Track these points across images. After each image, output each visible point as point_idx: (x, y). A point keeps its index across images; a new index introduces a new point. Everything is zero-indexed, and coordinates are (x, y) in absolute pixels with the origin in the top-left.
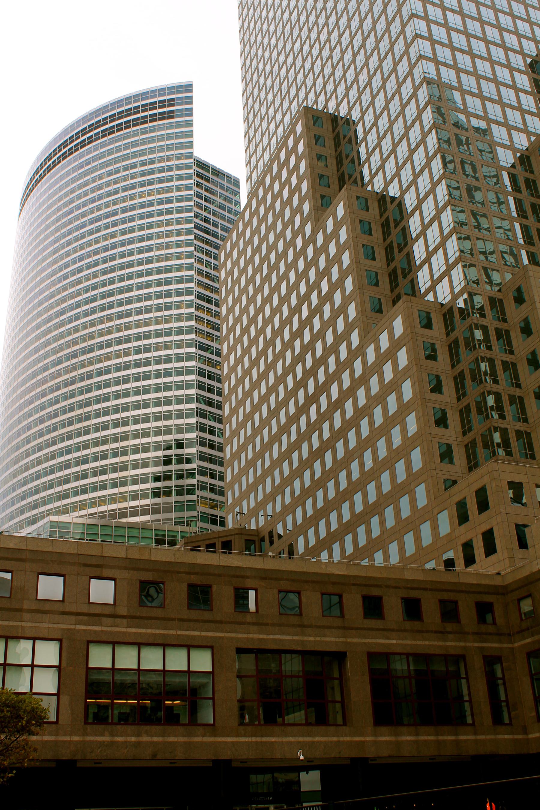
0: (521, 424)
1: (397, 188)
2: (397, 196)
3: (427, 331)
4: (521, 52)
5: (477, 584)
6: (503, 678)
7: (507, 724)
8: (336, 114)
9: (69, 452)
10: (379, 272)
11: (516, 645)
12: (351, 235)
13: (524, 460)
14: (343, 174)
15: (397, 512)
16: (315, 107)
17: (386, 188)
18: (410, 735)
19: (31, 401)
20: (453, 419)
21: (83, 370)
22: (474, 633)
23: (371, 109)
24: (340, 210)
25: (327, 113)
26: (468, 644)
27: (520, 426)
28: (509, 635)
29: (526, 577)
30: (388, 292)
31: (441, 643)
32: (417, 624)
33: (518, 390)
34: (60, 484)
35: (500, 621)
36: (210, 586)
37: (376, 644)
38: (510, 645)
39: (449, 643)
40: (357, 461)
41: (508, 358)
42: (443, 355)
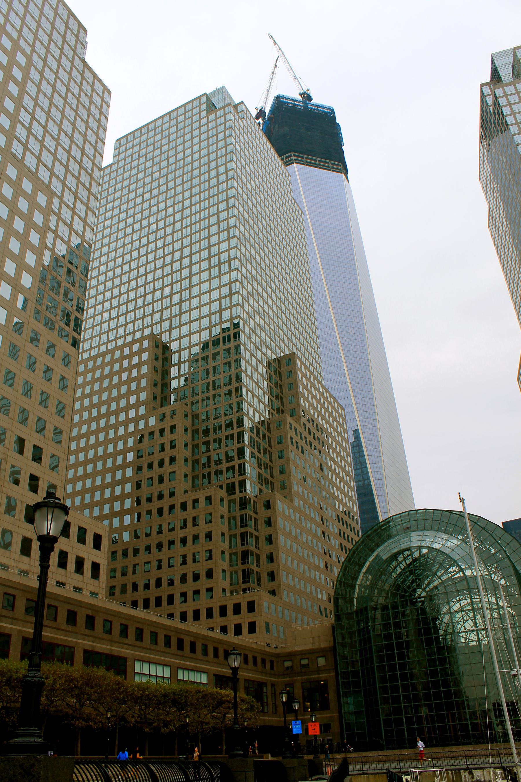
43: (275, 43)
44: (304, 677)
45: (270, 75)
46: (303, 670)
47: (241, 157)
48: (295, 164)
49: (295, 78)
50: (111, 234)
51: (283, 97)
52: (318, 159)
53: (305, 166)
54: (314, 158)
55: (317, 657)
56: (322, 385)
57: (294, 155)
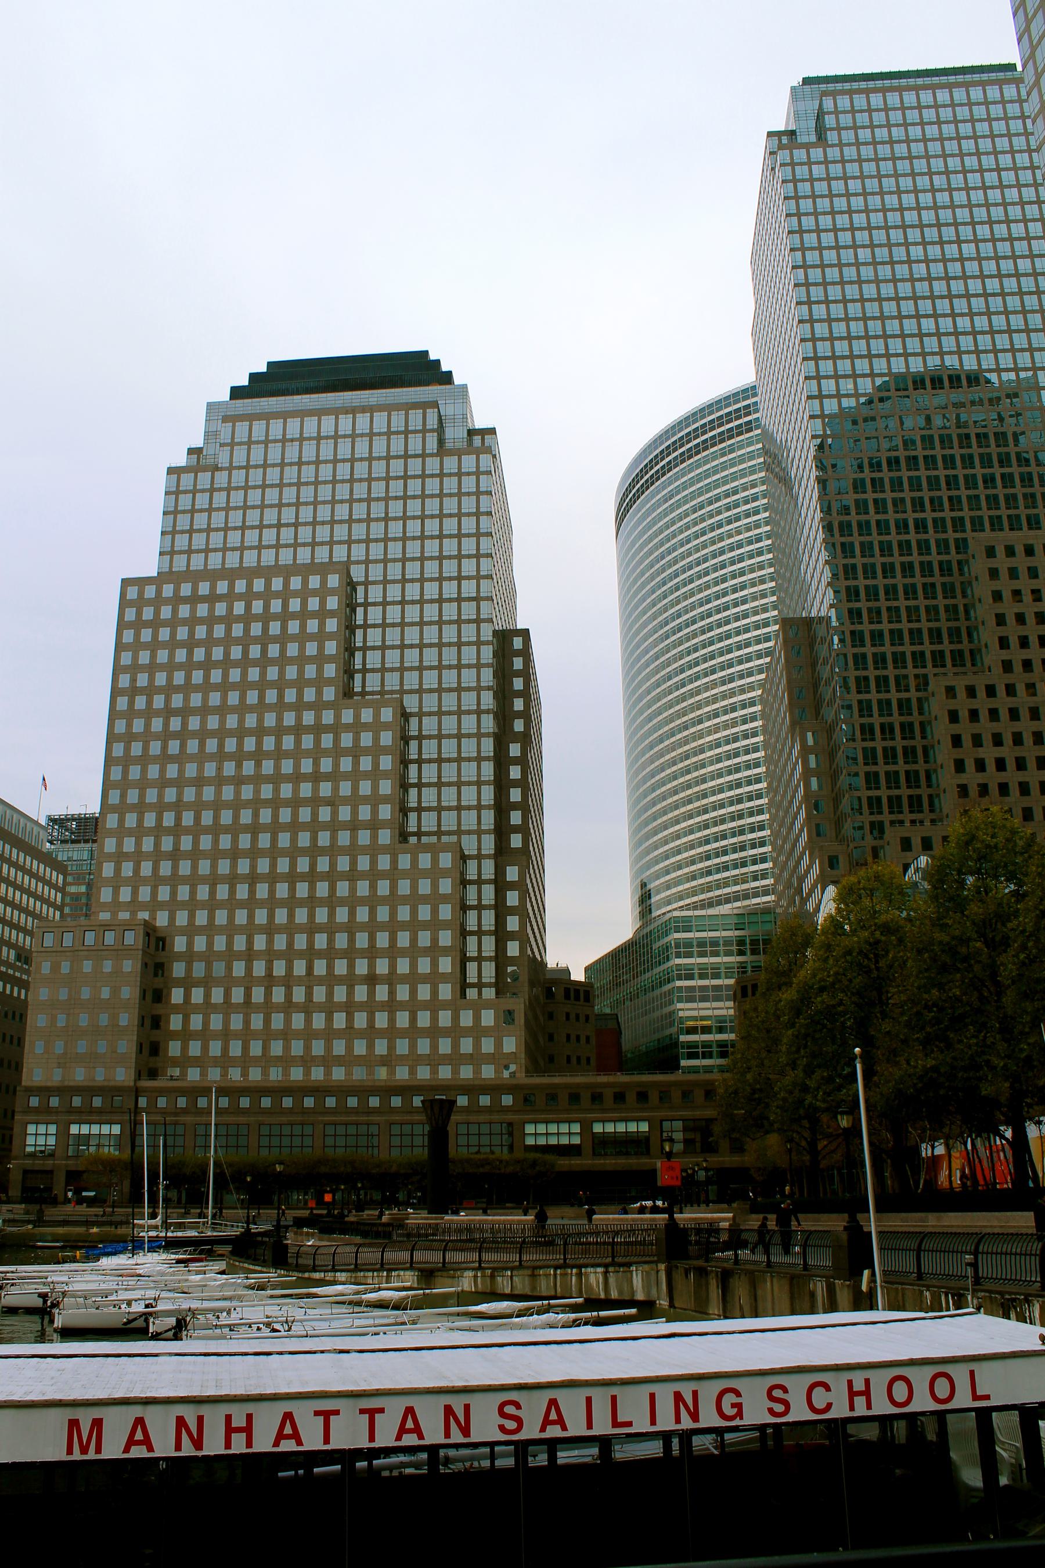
9: (688, 528)
19: (642, 573)
21: (697, 528)
34: (716, 840)
36: (1037, 624)
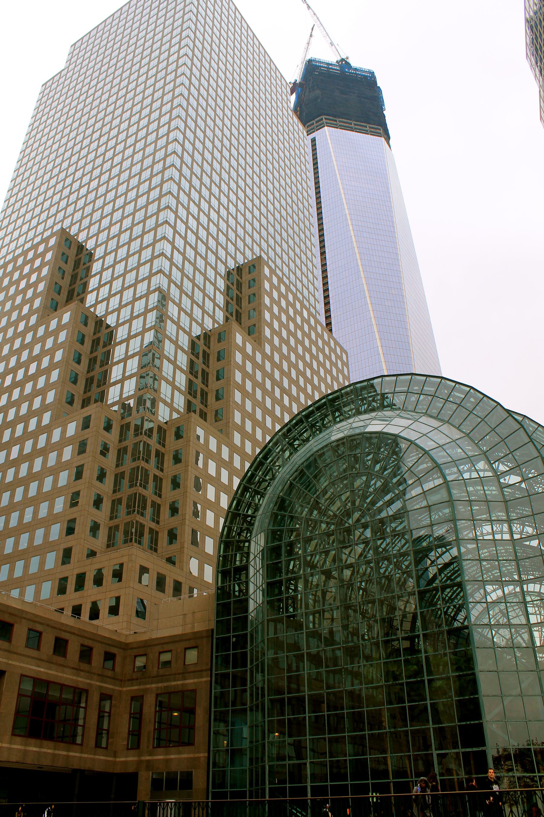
0: (154, 524)
1: (115, 320)
2: (112, 326)
3: (105, 433)
4: (225, 264)
5: (109, 638)
6: (110, 713)
7: (103, 748)
8: (84, 244)
10: (80, 375)
11: (125, 689)
12: (69, 339)
13: (150, 551)
14: (73, 290)
15: (42, 563)
16: (68, 230)
17: (105, 316)
18: (35, 746)
20: (106, 505)
22: (99, 675)
23: (41, 206)
24: (66, 317)
25: (76, 240)
26: (93, 682)
27: (153, 525)
28: (121, 680)
29: (146, 641)
30: (82, 392)
31: (74, 678)
32: (60, 660)
33: (159, 499)
35: (118, 669)
37: (30, 669)
38: (120, 689)
39: (80, 679)
40: (18, 513)
41: (158, 473)
42: (112, 455)
43: (309, 7)
44: (160, 685)
45: (305, 45)
46: (162, 672)
47: (302, 178)
48: (326, 127)
49: (332, 44)
50: (144, 233)
51: (315, 61)
52: (353, 122)
53: (338, 130)
54: (349, 121)
55: (186, 649)
56: (334, 340)
57: (326, 119)
